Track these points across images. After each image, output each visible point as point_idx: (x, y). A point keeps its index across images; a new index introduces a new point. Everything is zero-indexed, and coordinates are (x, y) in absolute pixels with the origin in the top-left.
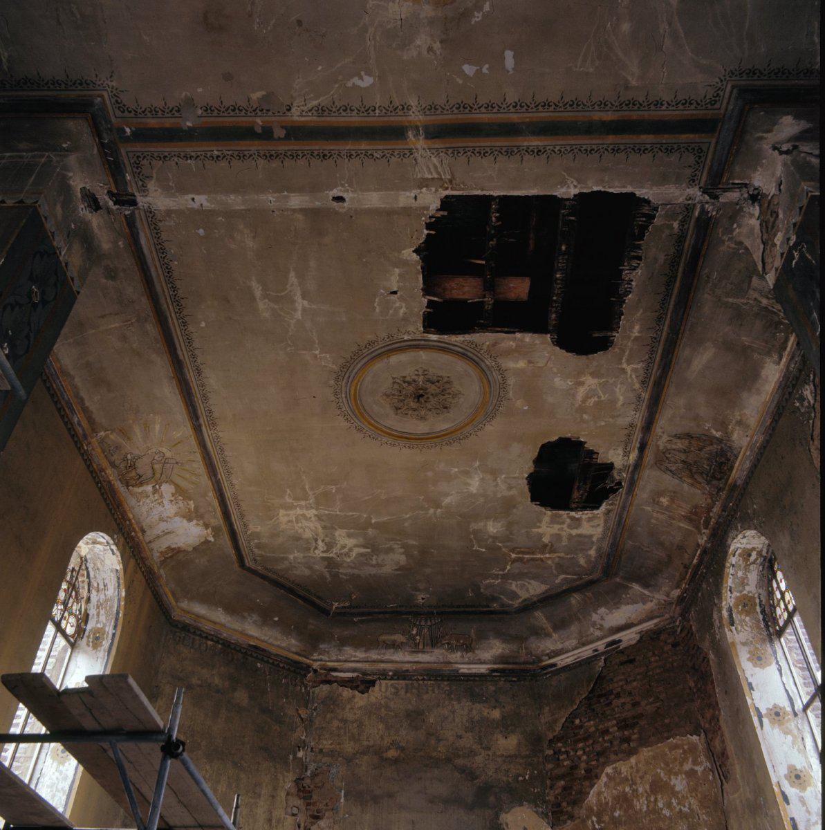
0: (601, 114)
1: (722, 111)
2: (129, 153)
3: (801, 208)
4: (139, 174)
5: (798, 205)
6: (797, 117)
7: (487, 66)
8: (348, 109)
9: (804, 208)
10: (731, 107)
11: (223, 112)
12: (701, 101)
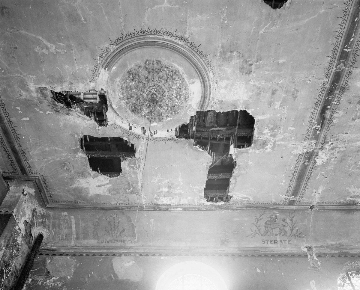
0: (17, 145)
1: (30, 175)
3: (7, 212)
4: (8, 117)
5: (8, 210)
6: (35, 192)
7: (21, 112)
9: (8, 213)
10: (32, 177)
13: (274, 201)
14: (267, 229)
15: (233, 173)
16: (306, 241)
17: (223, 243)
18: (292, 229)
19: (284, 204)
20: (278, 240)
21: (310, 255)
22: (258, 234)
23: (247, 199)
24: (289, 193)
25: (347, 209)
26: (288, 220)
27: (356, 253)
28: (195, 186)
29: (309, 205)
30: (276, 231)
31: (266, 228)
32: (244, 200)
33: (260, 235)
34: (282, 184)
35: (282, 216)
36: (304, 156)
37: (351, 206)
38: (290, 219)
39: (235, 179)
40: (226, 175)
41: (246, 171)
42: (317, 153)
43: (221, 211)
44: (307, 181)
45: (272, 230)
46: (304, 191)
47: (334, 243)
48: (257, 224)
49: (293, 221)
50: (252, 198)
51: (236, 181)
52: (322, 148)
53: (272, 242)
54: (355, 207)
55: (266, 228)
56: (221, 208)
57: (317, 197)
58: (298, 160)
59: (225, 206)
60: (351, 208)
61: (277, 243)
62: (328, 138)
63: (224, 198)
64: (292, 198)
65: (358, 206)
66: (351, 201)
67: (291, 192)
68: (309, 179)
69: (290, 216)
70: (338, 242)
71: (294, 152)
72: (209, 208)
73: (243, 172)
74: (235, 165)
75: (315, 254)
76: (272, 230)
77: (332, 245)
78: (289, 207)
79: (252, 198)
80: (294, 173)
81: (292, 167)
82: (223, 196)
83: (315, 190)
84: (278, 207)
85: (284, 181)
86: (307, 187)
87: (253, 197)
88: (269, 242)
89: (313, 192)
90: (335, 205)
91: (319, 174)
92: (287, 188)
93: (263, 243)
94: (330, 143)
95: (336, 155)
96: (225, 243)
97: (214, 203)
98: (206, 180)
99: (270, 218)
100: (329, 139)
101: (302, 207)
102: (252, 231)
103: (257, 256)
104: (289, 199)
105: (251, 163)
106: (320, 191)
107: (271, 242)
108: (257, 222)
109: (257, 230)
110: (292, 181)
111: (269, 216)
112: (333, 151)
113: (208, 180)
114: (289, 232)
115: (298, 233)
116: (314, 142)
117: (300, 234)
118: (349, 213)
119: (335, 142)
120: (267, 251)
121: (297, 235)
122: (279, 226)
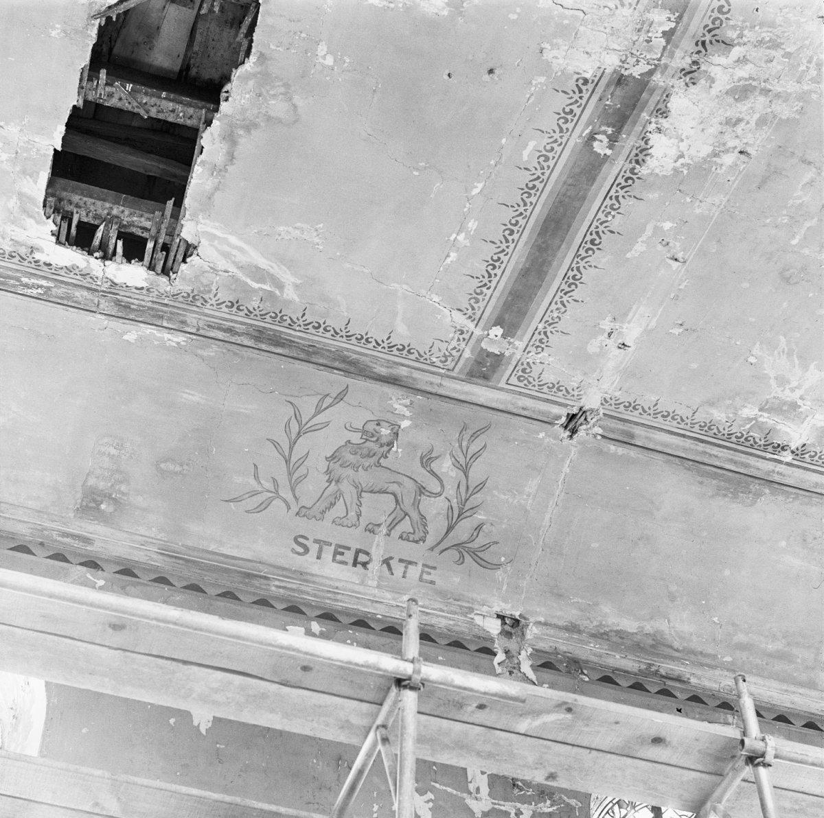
13: (403, 333)
14: (333, 486)
15: (223, 95)
17: (93, 505)
18: (456, 516)
19: (450, 364)
20: (377, 554)
21: (507, 652)
22: (285, 501)
24: (482, 304)
26: (445, 466)
28: (7, 124)
29: (566, 406)
30: (378, 508)
32: (256, 285)
33: (295, 509)
34: (461, 237)
35: (425, 438)
36: (600, 90)
37: (751, 454)
38: (457, 464)
40: (189, 105)
41: (295, 107)
44: (582, 252)
45: (360, 496)
46: (555, 315)
48: (291, 449)
49: (471, 474)
50: (297, 287)
51: (231, 157)
52: (691, 74)
53: (342, 554)
54: (769, 466)
55: (329, 481)
56: (125, 307)
57: (611, 364)
58: (567, 115)
59: (147, 301)
60: (747, 466)
61: (365, 565)
62: (731, 23)
63: (150, 245)
65: (780, 462)
66: (759, 426)
67: (493, 300)
69: (464, 444)
71: (555, 53)
72: (61, 291)
74: (242, 54)
75: (530, 650)
76: (360, 496)
77: (618, 632)
78: (467, 387)
79: (297, 287)
80: (529, 189)
81: (532, 144)
82: (145, 235)
83: (609, 318)
84: (416, 374)
85: (472, 225)
86: (576, 294)
87: (299, 282)
88: (328, 553)
89: (596, 330)
90: (684, 436)
91: (649, 231)
92: (481, 268)
93: (299, 554)
94: (737, 52)
95: (749, 138)
96: (103, 507)
98: (73, 99)
99: (364, 432)
100: (734, 27)
101: (529, 403)
102: (256, 477)
104: (480, 340)
105: (329, 61)
107: (339, 557)
109: (283, 479)
111: (360, 418)
112: (742, 108)
113: (81, 103)
114: (436, 527)
116: (660, 24)
117: (485, 548)
118: (735, 496)
119: (762, 52)
120: (308, 594)
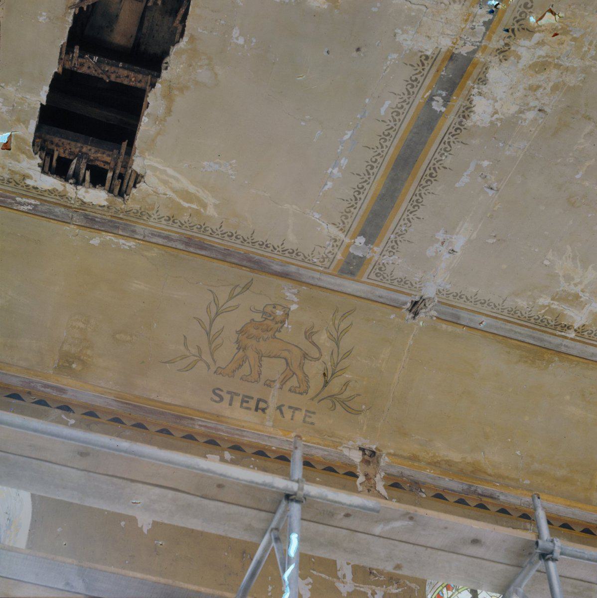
2: (370, 277)
8: (373, 164)
11: (395, 125)
12: (471, 297)
15: (164, 65)
16: (365, 427)
19: (327, 263)
20: (273, 402)
21: (366, 475)
23: (194, 206)
25: (532, 342)
27: (517, 502)
30: (273, 369)
31: (241, 347)
32: (186, 205)
33: (213, 368)
34: (335, 171)
39: (168, 96)
42: (486, 68)
43: (86, 233)
45: (260, 360)
47: (455, 456)
49: (341, 344)
51: (169, 111)
52: (503, 53)
53: (247, 402)
54: (559, 341)
55: (239, 349)
60: (542, 340)
61: (263, 410)
63: (110, 175)
64: (357, 248)
66: (551, 311)
68: (432, 177)
69: (337, 322)
70: (469, 459)
73: (203, 75)
74: (178, 36)
75: (383, 474)
78: (339, 281)
80: (385, 136)
82: (106, 167)
83: (442, 232)
84: (302, 271)
85: (344, 162)
90: (496, 318)
93: (216, 401)
96: (74, 366)
97: (68, 185)
98: (54, 68)
99: (264, 313)
102: (185, 345)
103: (179, 434)
104: (349, 246)
106: (459, 242)
107: (245, 405)
108: (213, 315)
110: (372, 167)
113: (60, 70)
114: (316, 382)
115: (347, 394)
116: (482, 16)
117: (350, 398)
121: (343, 403)
122: (289, 351)
